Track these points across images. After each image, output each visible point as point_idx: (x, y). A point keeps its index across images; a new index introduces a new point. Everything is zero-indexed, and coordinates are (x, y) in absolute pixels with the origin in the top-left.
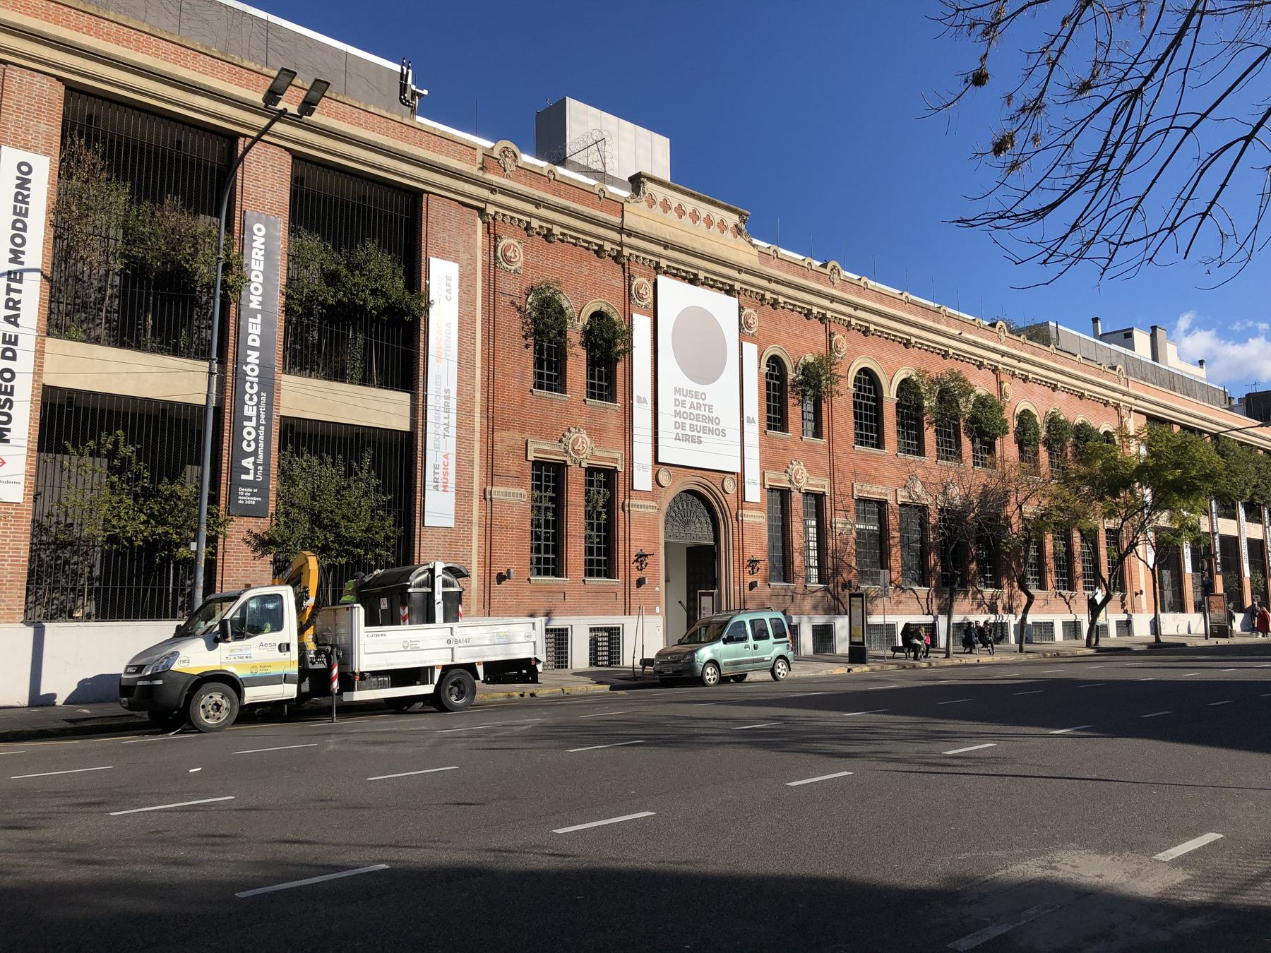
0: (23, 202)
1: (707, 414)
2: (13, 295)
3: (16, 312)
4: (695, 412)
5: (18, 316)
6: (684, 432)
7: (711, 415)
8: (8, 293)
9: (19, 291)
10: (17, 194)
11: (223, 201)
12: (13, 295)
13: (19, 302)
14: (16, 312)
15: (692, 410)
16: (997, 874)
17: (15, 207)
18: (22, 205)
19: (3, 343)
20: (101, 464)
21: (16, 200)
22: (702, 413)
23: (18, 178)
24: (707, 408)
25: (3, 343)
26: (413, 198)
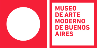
1: (76, 18)
4: (68, 18)
6: (61, 31)
7: (79, 18)
13: (64, 35)
15: (67, 17)
22: (73, 18)
24: (76, 14)
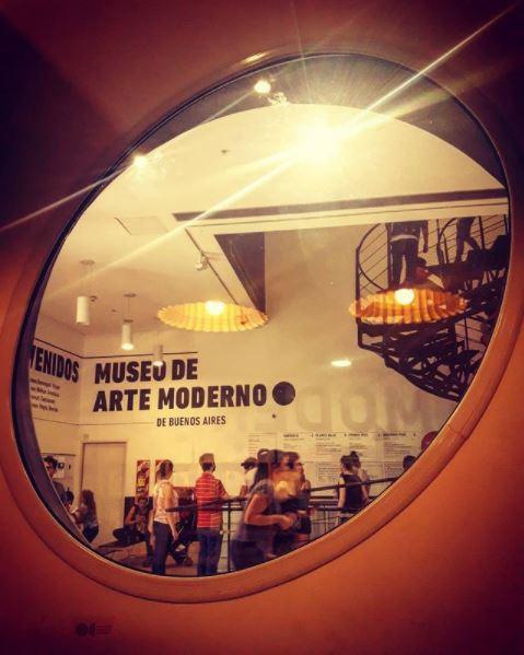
0: (224, 396)
2: (125, 398)
3: (108, 407)
5: (105, 409)
8: (126, 392)
9: (130, 407)
10: (230, 388)
11: (49, 211)
12: (125, 398)
13: (120, 408)
14: (108, 407)
16: (136, 253)
17: (216, 388)
18: (219, 397)
19: (210, 388)
20: (193, 485)
21: (224, 389)
23: (247, 387)
25: (210, 388)
26: (353, 453)
